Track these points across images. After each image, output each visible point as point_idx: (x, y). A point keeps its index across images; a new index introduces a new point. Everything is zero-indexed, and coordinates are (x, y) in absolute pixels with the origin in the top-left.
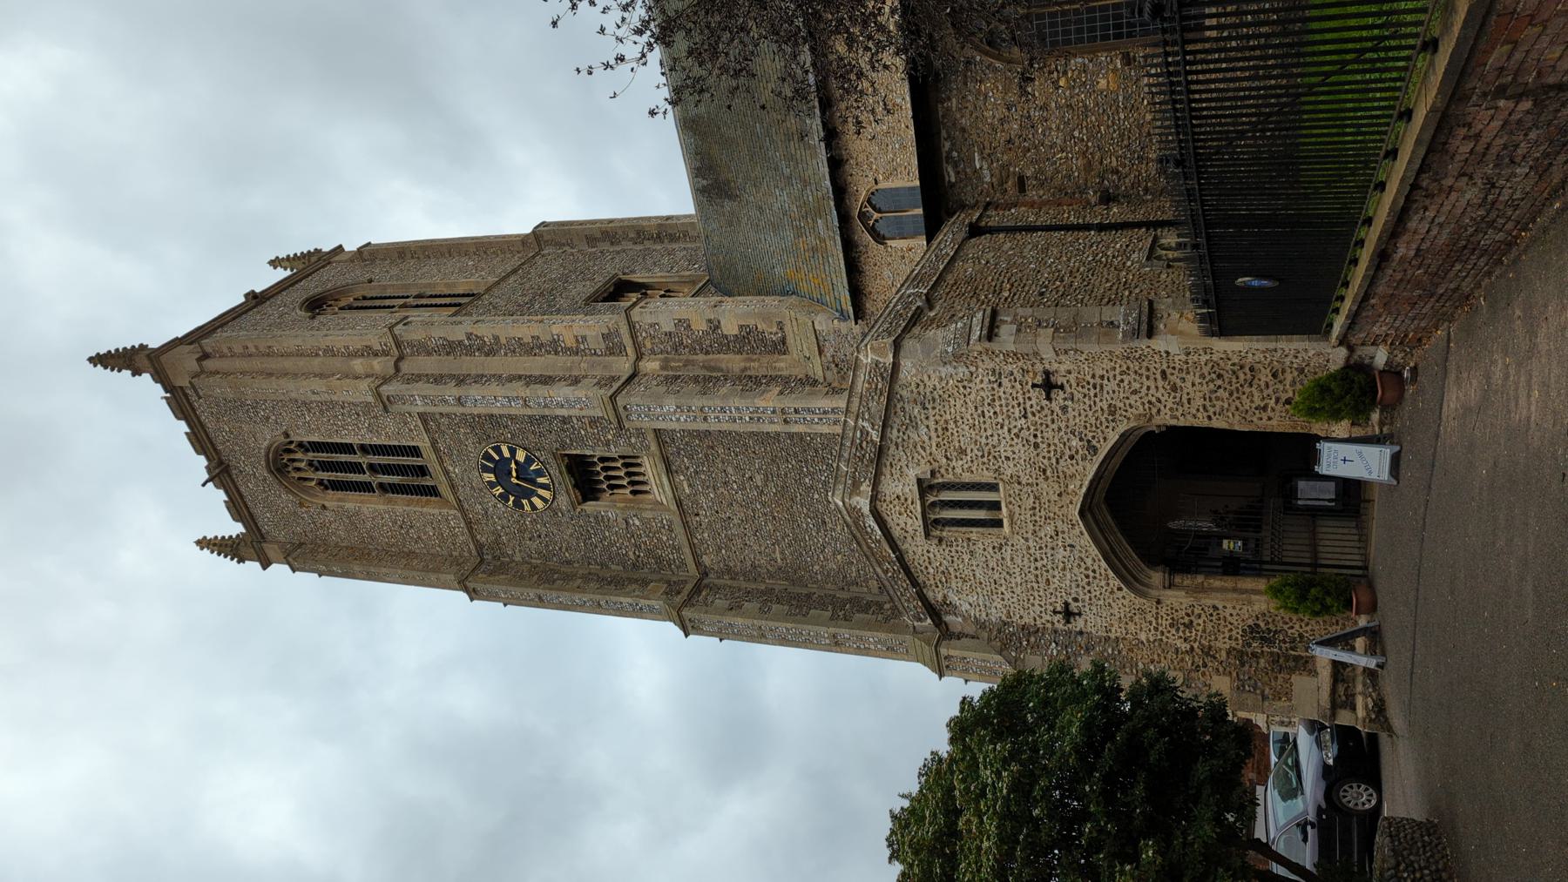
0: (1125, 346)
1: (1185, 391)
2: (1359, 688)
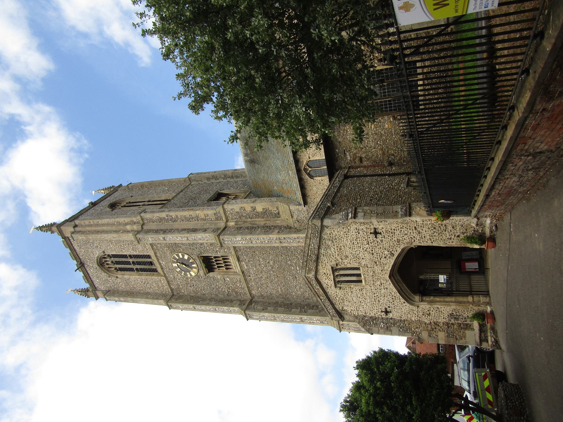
0: (402, 219)
1: (423, 233)
2: (489, 334)
